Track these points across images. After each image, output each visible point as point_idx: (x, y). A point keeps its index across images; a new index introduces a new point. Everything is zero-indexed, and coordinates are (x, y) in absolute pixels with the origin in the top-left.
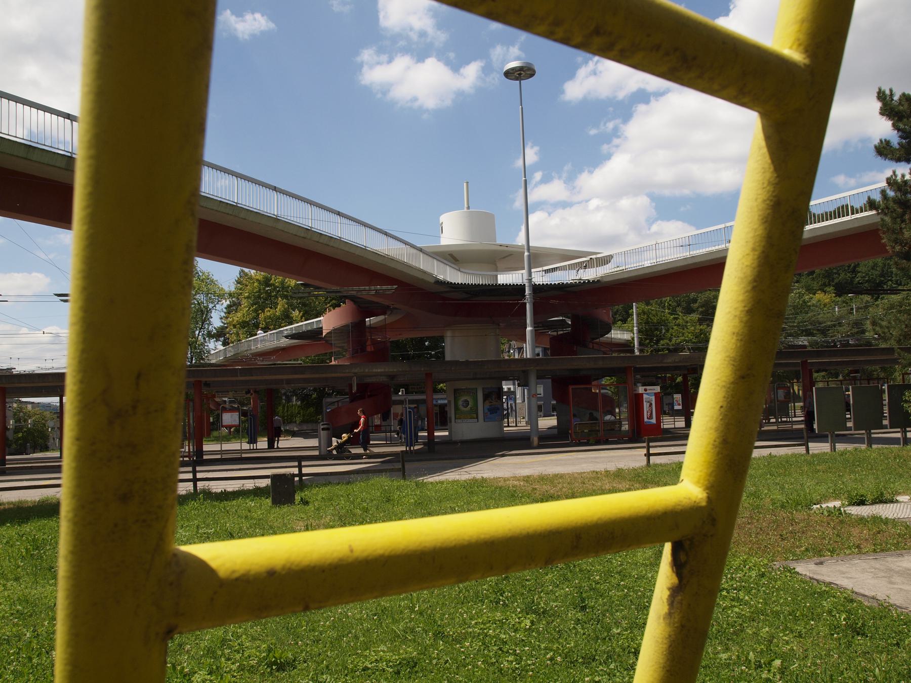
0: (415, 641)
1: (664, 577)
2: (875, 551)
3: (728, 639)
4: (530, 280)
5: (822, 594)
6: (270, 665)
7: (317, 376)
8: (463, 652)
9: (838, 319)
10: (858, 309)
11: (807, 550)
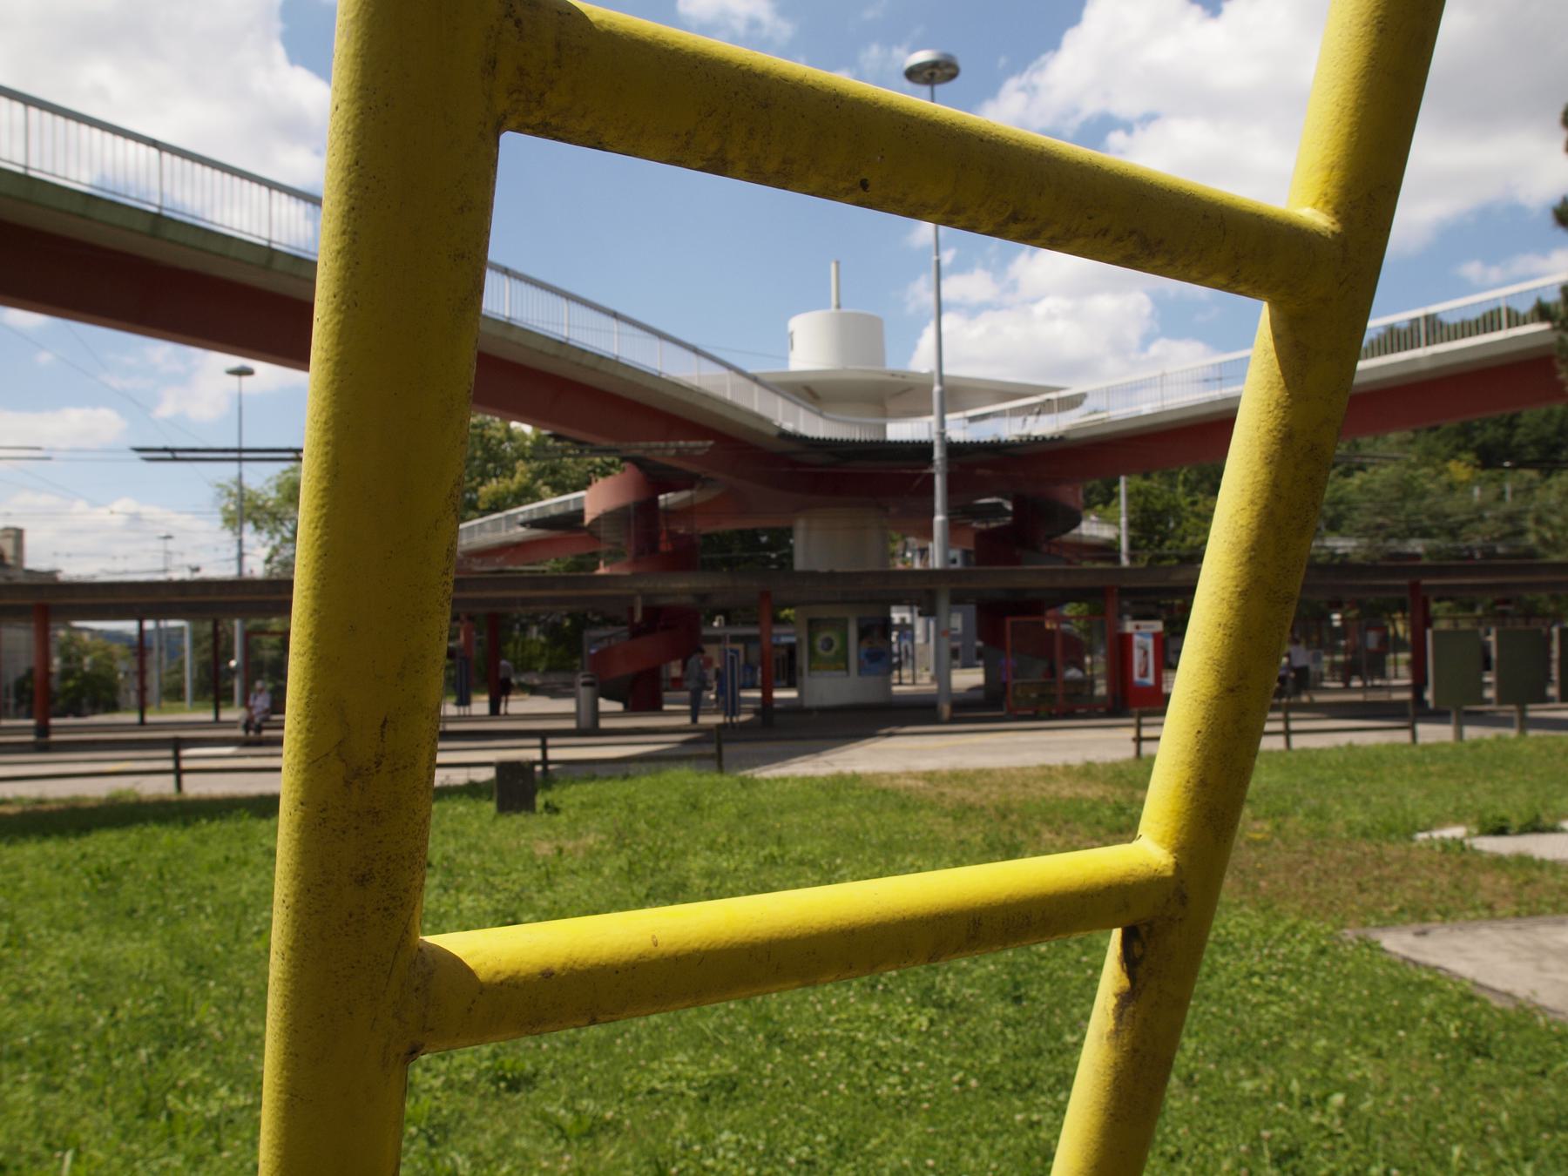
0: (734, 1048)
1: (1111, 978)
2: (1517, 915)
3: (1258, 1058)
4: (942, 434)
5: (1422, 987)
6: (495, 1081)
7: (574, 593)
8: (814, 1069)
9: (1480, 509)
10: (1514, 493)
11: (1402, 910)
